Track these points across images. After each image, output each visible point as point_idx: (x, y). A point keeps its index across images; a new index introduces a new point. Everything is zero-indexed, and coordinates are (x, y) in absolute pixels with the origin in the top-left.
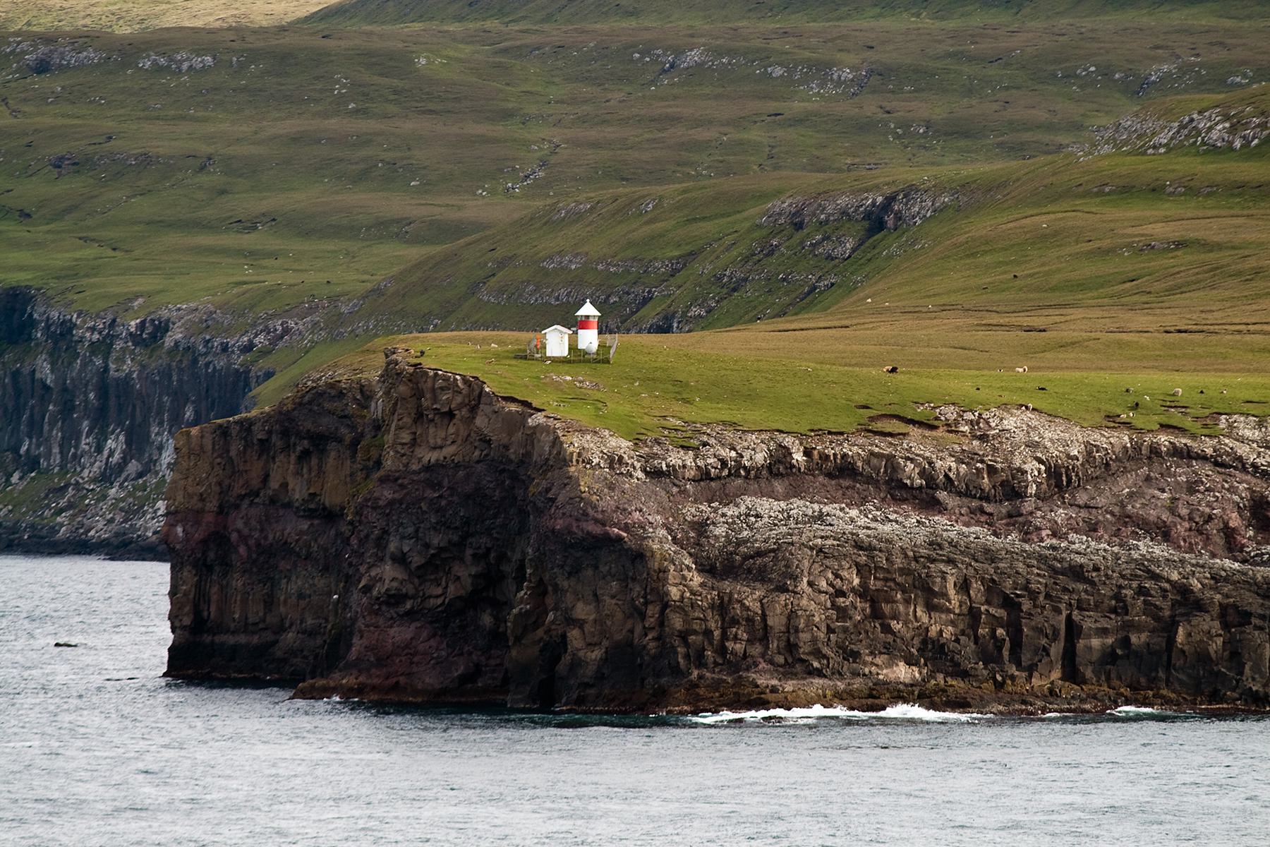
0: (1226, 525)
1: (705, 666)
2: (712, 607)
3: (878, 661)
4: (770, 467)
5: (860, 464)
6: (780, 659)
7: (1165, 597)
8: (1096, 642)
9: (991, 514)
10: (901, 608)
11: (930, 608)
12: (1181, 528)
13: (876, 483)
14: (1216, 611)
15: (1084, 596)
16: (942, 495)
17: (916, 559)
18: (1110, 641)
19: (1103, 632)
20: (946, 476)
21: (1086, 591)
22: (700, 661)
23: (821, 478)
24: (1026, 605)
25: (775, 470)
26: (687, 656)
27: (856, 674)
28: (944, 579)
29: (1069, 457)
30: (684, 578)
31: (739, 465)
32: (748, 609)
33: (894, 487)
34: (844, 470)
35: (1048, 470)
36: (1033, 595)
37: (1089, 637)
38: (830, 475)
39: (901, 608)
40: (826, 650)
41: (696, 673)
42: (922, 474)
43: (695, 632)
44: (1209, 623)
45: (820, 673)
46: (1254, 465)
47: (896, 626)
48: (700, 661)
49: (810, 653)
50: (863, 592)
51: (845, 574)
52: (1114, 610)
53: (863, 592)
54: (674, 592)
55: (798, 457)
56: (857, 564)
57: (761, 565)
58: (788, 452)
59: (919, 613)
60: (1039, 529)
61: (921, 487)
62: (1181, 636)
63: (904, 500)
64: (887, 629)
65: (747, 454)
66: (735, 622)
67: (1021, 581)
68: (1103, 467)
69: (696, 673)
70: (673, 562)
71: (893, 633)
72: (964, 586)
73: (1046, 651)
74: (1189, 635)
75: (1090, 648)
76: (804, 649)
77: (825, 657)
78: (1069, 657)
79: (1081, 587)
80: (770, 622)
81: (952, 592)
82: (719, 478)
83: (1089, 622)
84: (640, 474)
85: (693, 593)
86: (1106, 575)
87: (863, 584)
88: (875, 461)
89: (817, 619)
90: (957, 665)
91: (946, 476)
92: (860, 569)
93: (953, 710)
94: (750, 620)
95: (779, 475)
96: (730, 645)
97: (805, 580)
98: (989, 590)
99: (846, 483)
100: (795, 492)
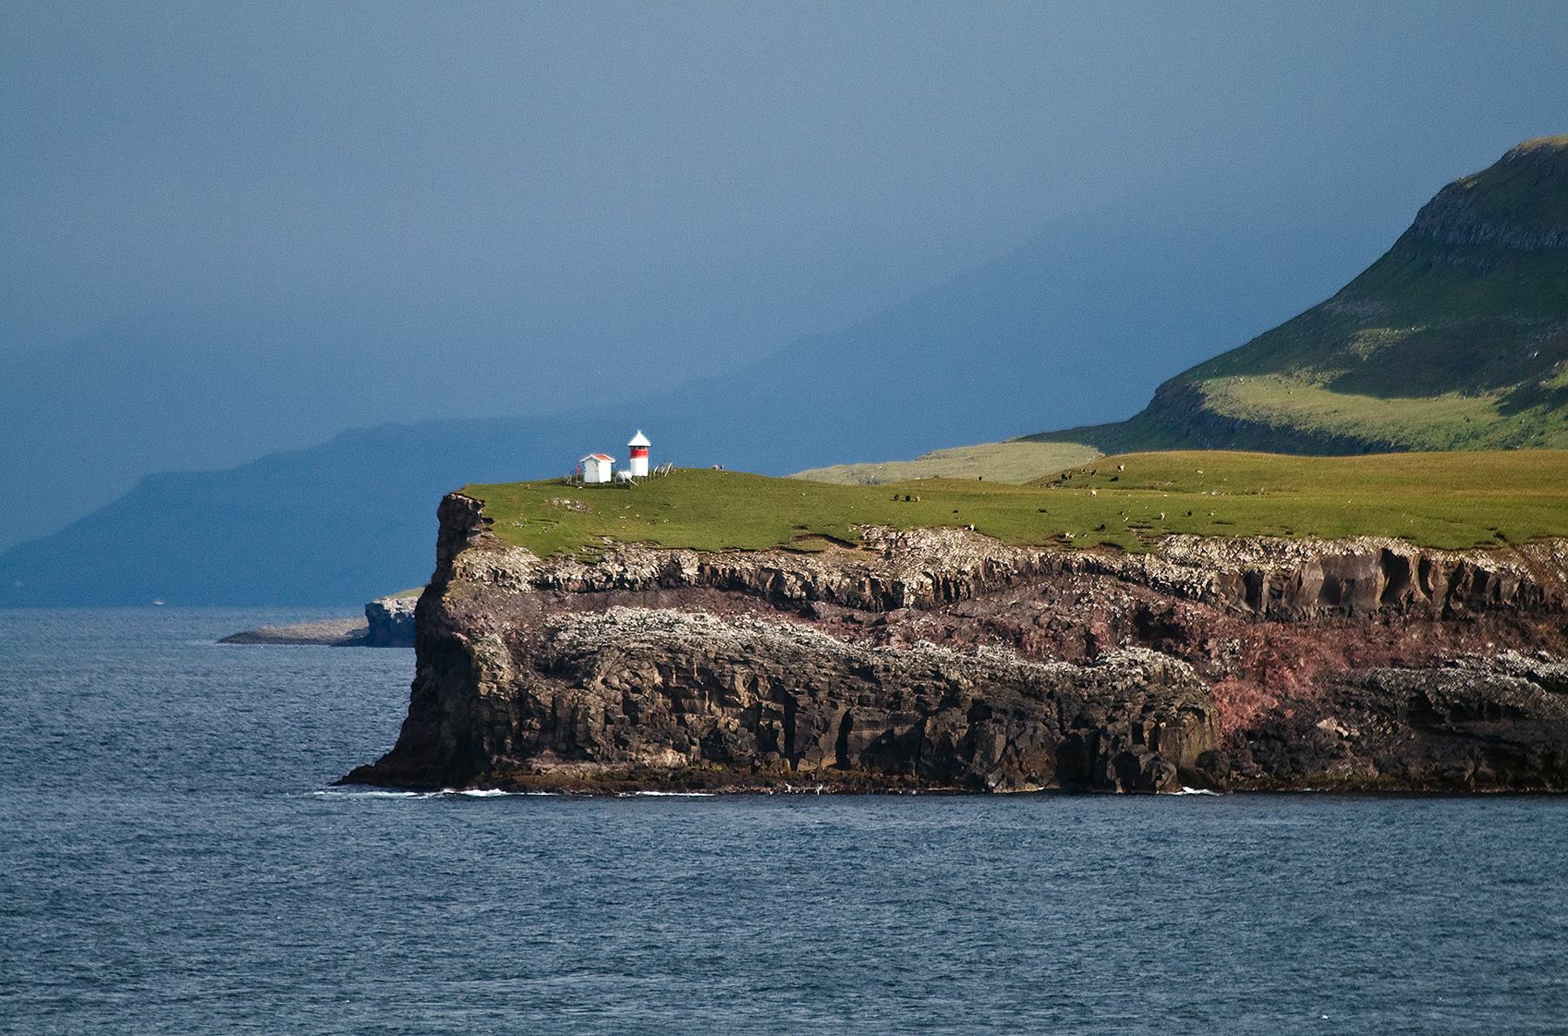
0: (1088, 633)
1: (504, 752)
2: (513, 700)
3: (650, 748)
4: (659, 581)
5: (746, 578)
6: (563, 746)
7: (937, 694)
8: (866, 733)
9: (860, 623)
10: (698, 702)
11: (723, 703)
12: (1035, 636)
13: (763, 595)
14: (968, 706)
15: (867, 693)
16: (819, 606)
17: (715, 660)
18: (880, 732)
19: (873, 724)
20: (828, 588)
21: (871, 689)
22: (501, 749)
23: (712, 591)
24: (803, 700)
25: (664, 583)
26: (491, 744)
27: (623, 759)
28: (733, 678)
29: (961, 572)
30: (495, 676)
31: (622, 580)
32: (539, 702)
33: (777, 599)
34: (733, 583)
35: (935, 583)
36: (813, 692)
37: (861, 728)
38: (719, 587)
39: (698, 702)
40: (599, 739)
41: (495, 758)
42: (805, 586)
43: (499, 723)
44: (957, 716)
45: (591, 759)
46: (1155, 579)
47: (689, 718)
48: (501, 749)
49: (584, 741)
50: (665, 689)
51: (643, 673)
52: (889, 706)
53: (665, 689)
54: (483, 688)
55: (690, 571)
56: (658, 665)
57: (571, 667)
58: (678, 567)
59: (713, 707)
60: (890, 635)
61: (800, 598)
62: (928, 729)
63: (786, 610)
64: (682, 721)
65: (631, 569)
66: (530, 715)
67: (804, 679)
68: (994, 580)
69: (495, 758)
70: (485, 661)
71: (686, 725)
72: (753, 685)
73: (816, 740)
74: (935, 727)
75: (860, 739)
76: (580, 736)
77: (596, 744)
78: (842, 747)
79: (867, 685)
80: (559, 713)
81: (741, 689)
82: (603, 590)
83: (860, 717)
84: (525, 586)
85: (499, 689)
86: (895, 676)
87: (665, 683)
88: (764, 575)
89: (592, 711)
90: (725, 751)
91: (828, 588)
92: (661, 669)
93: (382, 786)
94: (542, 713)
95: (668, 587)
96: (526, 734)
97: (600, 678)
98: (774, 687)
99: (737, 594)
100: (681, 604)
